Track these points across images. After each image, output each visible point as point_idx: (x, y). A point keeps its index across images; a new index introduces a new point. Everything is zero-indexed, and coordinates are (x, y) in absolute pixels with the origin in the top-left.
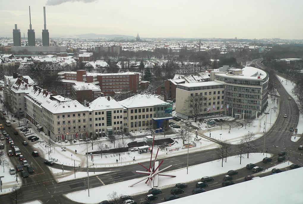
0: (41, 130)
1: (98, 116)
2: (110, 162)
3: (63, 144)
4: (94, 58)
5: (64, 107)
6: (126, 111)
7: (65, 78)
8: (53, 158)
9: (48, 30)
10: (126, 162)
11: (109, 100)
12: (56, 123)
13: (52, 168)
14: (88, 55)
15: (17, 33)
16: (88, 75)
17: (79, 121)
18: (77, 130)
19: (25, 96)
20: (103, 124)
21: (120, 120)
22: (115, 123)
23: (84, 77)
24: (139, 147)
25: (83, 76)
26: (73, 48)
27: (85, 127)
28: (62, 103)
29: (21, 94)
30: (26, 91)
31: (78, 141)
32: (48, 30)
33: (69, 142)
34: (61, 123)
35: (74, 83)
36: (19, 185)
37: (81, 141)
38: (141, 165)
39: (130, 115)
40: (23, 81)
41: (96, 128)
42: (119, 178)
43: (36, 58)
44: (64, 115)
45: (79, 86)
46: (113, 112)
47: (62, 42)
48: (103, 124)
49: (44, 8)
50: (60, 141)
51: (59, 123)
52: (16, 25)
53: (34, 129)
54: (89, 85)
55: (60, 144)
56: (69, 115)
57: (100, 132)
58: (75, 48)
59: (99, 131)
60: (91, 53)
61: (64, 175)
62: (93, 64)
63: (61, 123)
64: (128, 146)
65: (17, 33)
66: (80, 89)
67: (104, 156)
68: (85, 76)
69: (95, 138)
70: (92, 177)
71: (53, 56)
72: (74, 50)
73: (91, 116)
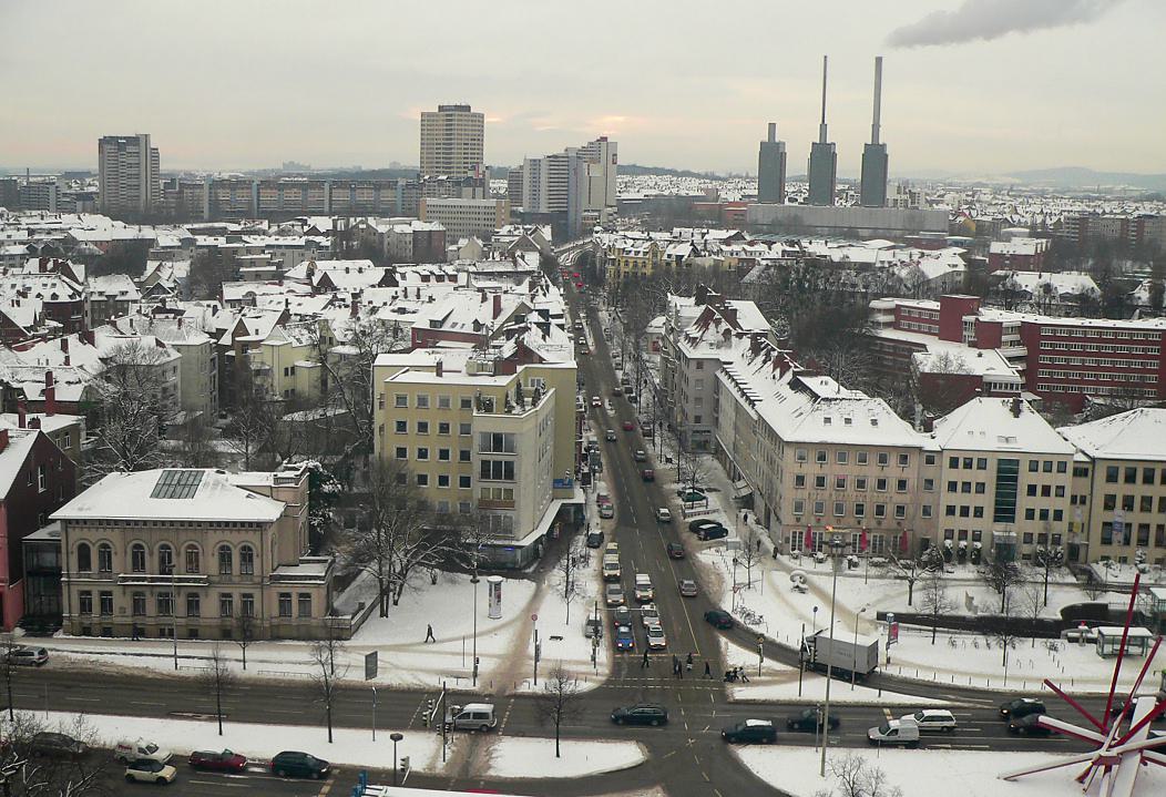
0: (747, 502)
1: (960, 475)
2: (955, 666)
3: (807, 564)
4: (1046, 262)
5: (828, 420)
6: (1086, 470)
7: (895, 325)
8: (749, 607)
9: (884, 146)
10: (1026, 680)
11: (1017, 416)
12: (789, 481)
13: (730, 644)
14: (1025, 246)
15: (772, 154)
16: (981, 319)
17: (882, 484)
18: (868, 520)
19: (718, 373)
20: (979, 512)
21: (1052, 503)
22: (1030, 514)
23: (966, 323)
24: (1103, 629)
25: (965, 318)
26: (979, 218)
27: (900, 510)
28: (824, 406)
29: (705, 363)
30: (723, 355)
31: (863, 562)
32: (884, 146)
33: (830, 559)
34: (810, 481)
35: (924, 346)
36: (600, 678)
37: (876, 565)
38: (1075, 705)
39: (1102, 488)
40: (717, 316)
41: (946, 523)
42: (971, 734)
43: (817, 247)
44: (822, 451)
45: (937, 355)
46: (1024, 467)
47: (943, 196)
48: (979, 512)
49: (879, 61)
50: (796, 552)
51: (800, 480)
52: (772, 126)
53: (726, 499)
54: (980, 355)
55: (793, 564)
56: (843, 451)
57: (963, 544)
58: (985, 218)
59: (960, 539)
60: (1044, 241)
61: (763, 678)
62: (1028, 281)
63: (810, 481)
64: (1060, 617)
65: (772, 154)
66: (929, 364)
67: (943, 638)
68: (971, 318)
69: (936, 564)
70: (871, 710)
71: (893, 244)
72: (980, 225)
73: (930, 472)
